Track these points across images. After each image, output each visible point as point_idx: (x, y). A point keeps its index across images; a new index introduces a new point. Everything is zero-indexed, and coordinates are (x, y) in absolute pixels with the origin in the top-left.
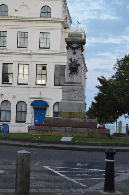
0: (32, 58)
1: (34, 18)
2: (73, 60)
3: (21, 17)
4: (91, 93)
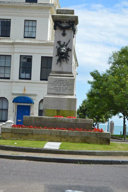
0: (15, 48)
1: (18, 3)
2: (62, 43)
3: (3, 2)
4: (81, 93)
